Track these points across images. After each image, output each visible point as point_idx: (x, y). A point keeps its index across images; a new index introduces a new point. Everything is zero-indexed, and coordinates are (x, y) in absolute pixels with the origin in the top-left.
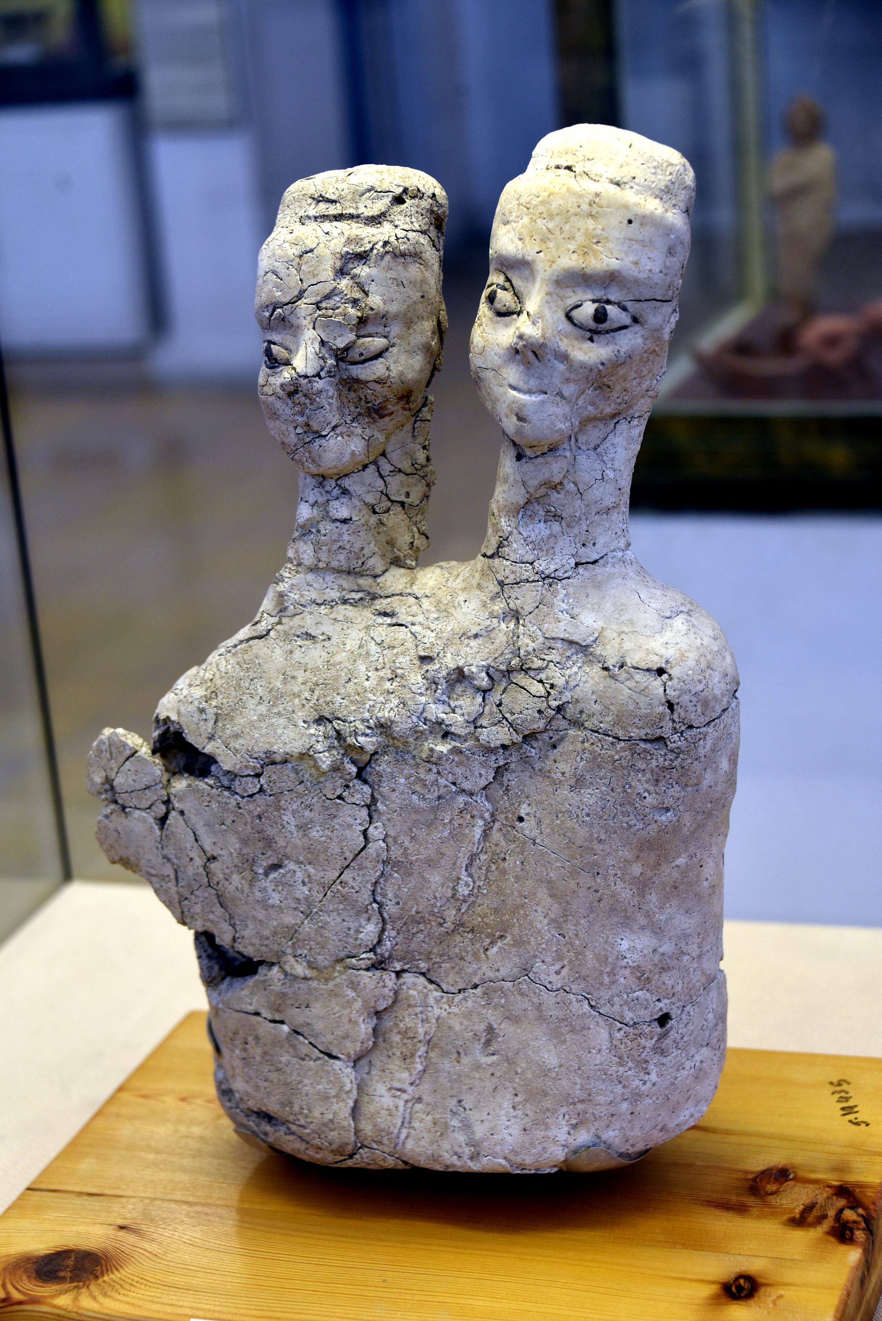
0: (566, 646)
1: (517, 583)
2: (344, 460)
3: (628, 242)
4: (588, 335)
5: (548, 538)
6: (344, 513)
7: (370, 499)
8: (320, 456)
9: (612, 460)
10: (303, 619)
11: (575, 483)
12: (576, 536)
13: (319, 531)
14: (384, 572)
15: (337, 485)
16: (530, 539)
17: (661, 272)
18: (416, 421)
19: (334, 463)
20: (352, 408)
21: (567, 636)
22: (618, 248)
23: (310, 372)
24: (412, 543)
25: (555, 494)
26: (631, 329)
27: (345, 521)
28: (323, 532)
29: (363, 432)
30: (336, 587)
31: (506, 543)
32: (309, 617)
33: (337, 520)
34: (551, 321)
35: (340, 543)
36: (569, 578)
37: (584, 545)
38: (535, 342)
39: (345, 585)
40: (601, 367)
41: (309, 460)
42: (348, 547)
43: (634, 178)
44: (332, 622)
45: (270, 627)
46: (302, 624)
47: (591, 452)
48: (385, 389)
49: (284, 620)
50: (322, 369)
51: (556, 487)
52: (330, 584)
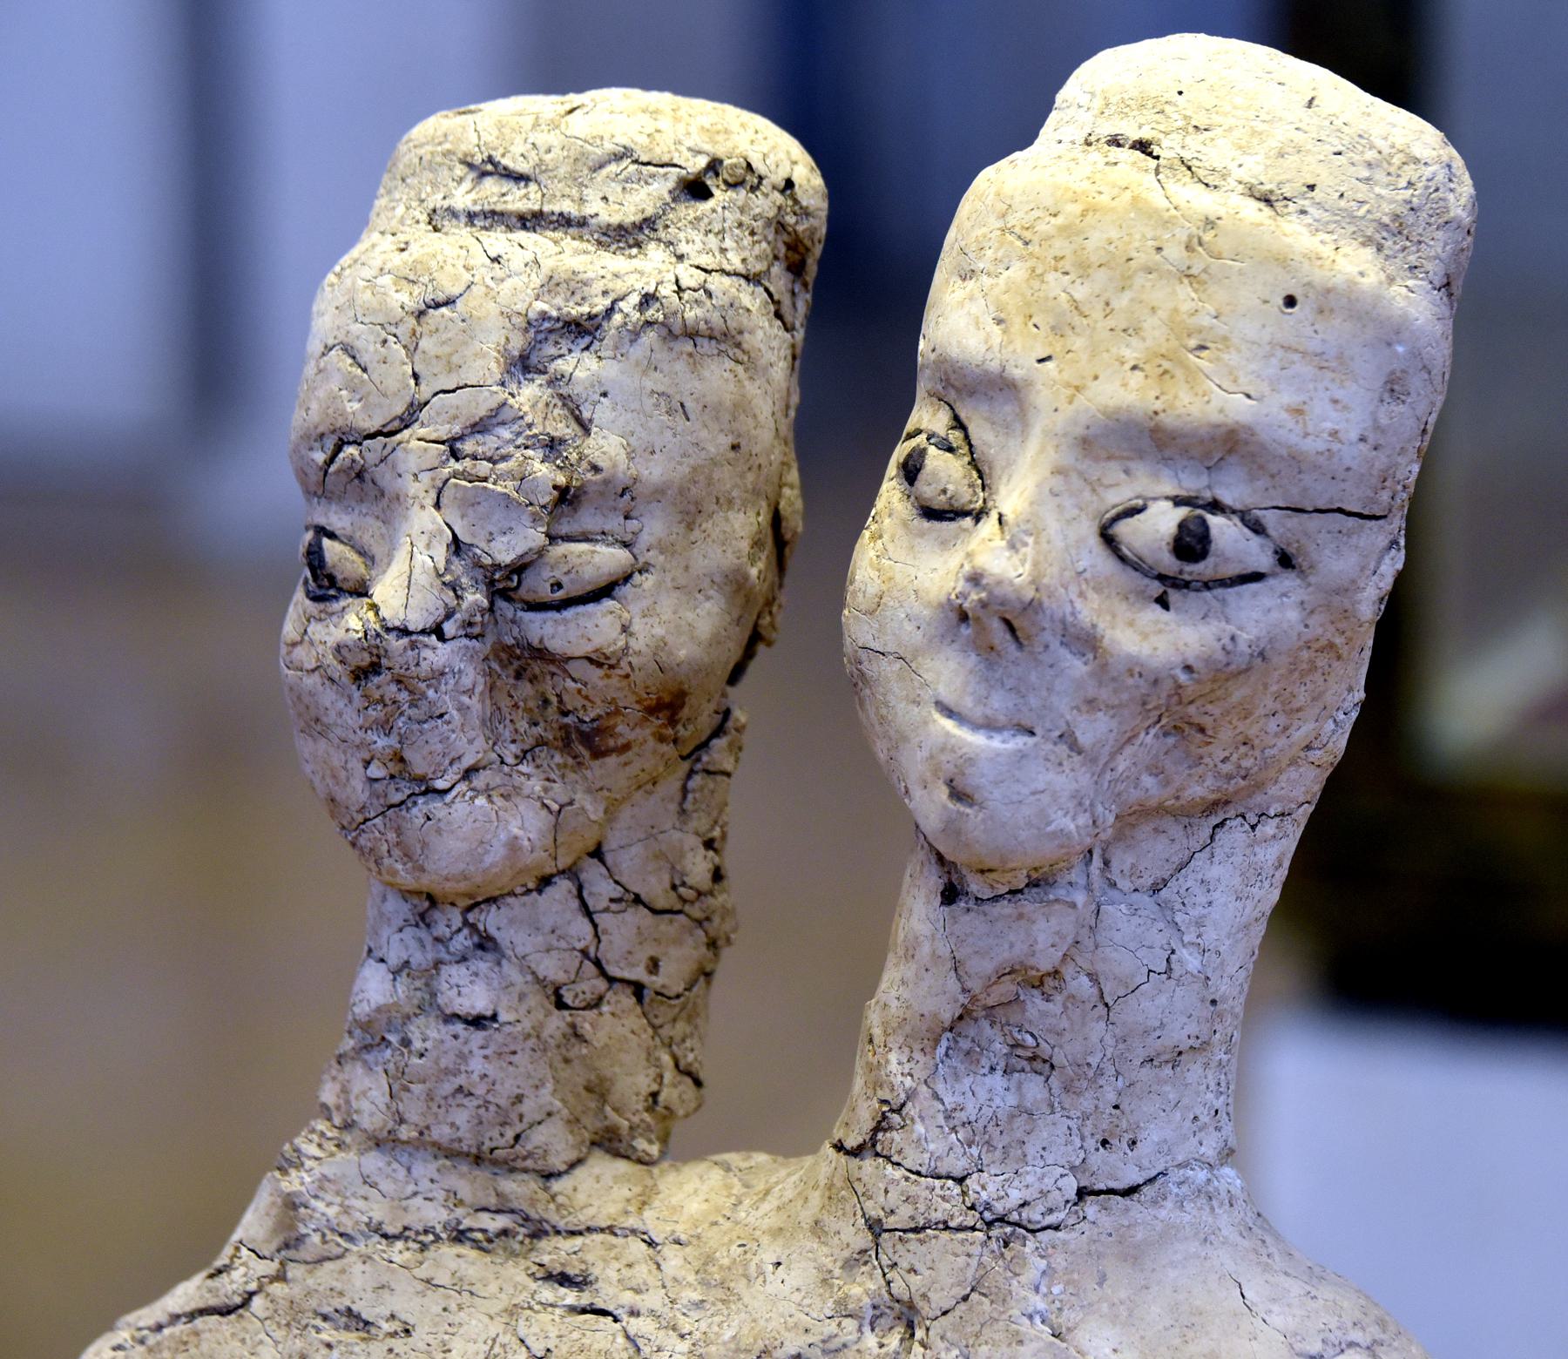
1: (916, 1230)
2: (488, 860)
3: (1280, 353)
4: (1156, 588)
5: (1012, 1117)
6: (477, 1000)
7: (551, 968)
9: (1199, 923)
10: (343, 1271)
13: (406, 1042)
14: (572, 1166)
16: (962, 1116)
17: (1362, 439)
19: (462, 866)
20: (523, 725)
22: (1253, 366)
23: (416, 621)
24: (654, 1095)
25: (1038, 1000)
26: (1271, 582)
27: (477, 1022)
28: (417, 1045)
29: (546, 790)
32: (359, 1267)
34: (1059, 544)
35: (461, 1080)
36: (1057, 1228)
37: (1105, 1143)
38: (1013, 596)
39: (465, 1191)
40: (1183, 678)
42: (480, 1090)
43: (1312, 187)
44: (420, 1286)
45: (253, 1286)
46: (338, 1286)
47: (1144, 899)
48: (615, 681)
49: (294, 1271)
51: (1044, 982)
52: (425, 1185)
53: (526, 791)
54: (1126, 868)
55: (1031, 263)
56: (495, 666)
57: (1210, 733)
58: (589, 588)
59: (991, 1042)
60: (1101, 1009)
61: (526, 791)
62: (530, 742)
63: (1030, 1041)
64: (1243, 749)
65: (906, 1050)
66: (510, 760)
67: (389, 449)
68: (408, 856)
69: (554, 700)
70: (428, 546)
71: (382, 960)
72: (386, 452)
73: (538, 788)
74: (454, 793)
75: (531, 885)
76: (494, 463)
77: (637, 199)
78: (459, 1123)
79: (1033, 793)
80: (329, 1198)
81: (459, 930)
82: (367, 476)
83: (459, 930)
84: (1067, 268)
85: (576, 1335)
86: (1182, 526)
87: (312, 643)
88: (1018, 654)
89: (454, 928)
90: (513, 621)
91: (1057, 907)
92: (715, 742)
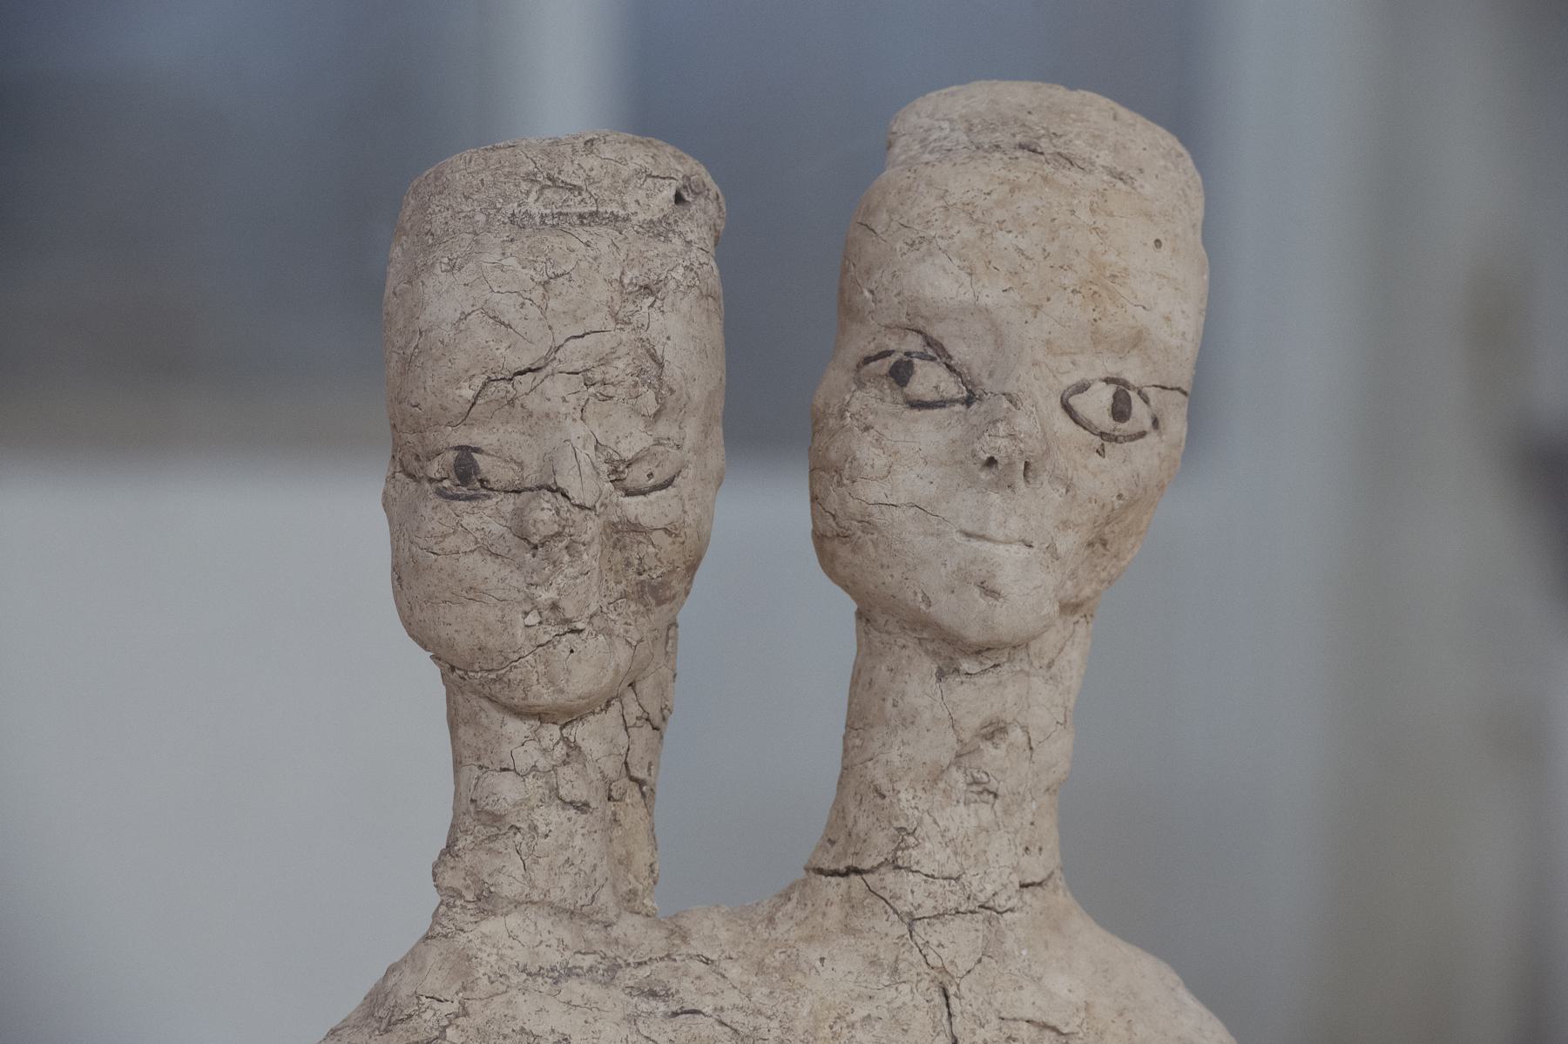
0: (1034, 1030)
2: (605, 681)
4: (1097, 441)
5: (976, 835)
8: (569, 671)
10: (509, 1002)
11: (1025, 729)
12: (1016, 832)
21: (1038, 1014)
28: (542, 829)
30: (554, 943)
31: (911, 840)
32: (521, 999)
35: (568, 854)
36: (1012, 910)
42: (577, 862)
44: (565, 1008)
45: (445, 1023)
46: (510, 1012)
49: (473, 1007)
51: (994, 731)
52: (545, 936)
55: (979, 227)
60: (1028, 752)
62: (616, 595)
63: (985, 778)
67: (538, 381)
78: (564, 889)
80: (488, 950)
85: (685, 1028)
86: (1114, 397)
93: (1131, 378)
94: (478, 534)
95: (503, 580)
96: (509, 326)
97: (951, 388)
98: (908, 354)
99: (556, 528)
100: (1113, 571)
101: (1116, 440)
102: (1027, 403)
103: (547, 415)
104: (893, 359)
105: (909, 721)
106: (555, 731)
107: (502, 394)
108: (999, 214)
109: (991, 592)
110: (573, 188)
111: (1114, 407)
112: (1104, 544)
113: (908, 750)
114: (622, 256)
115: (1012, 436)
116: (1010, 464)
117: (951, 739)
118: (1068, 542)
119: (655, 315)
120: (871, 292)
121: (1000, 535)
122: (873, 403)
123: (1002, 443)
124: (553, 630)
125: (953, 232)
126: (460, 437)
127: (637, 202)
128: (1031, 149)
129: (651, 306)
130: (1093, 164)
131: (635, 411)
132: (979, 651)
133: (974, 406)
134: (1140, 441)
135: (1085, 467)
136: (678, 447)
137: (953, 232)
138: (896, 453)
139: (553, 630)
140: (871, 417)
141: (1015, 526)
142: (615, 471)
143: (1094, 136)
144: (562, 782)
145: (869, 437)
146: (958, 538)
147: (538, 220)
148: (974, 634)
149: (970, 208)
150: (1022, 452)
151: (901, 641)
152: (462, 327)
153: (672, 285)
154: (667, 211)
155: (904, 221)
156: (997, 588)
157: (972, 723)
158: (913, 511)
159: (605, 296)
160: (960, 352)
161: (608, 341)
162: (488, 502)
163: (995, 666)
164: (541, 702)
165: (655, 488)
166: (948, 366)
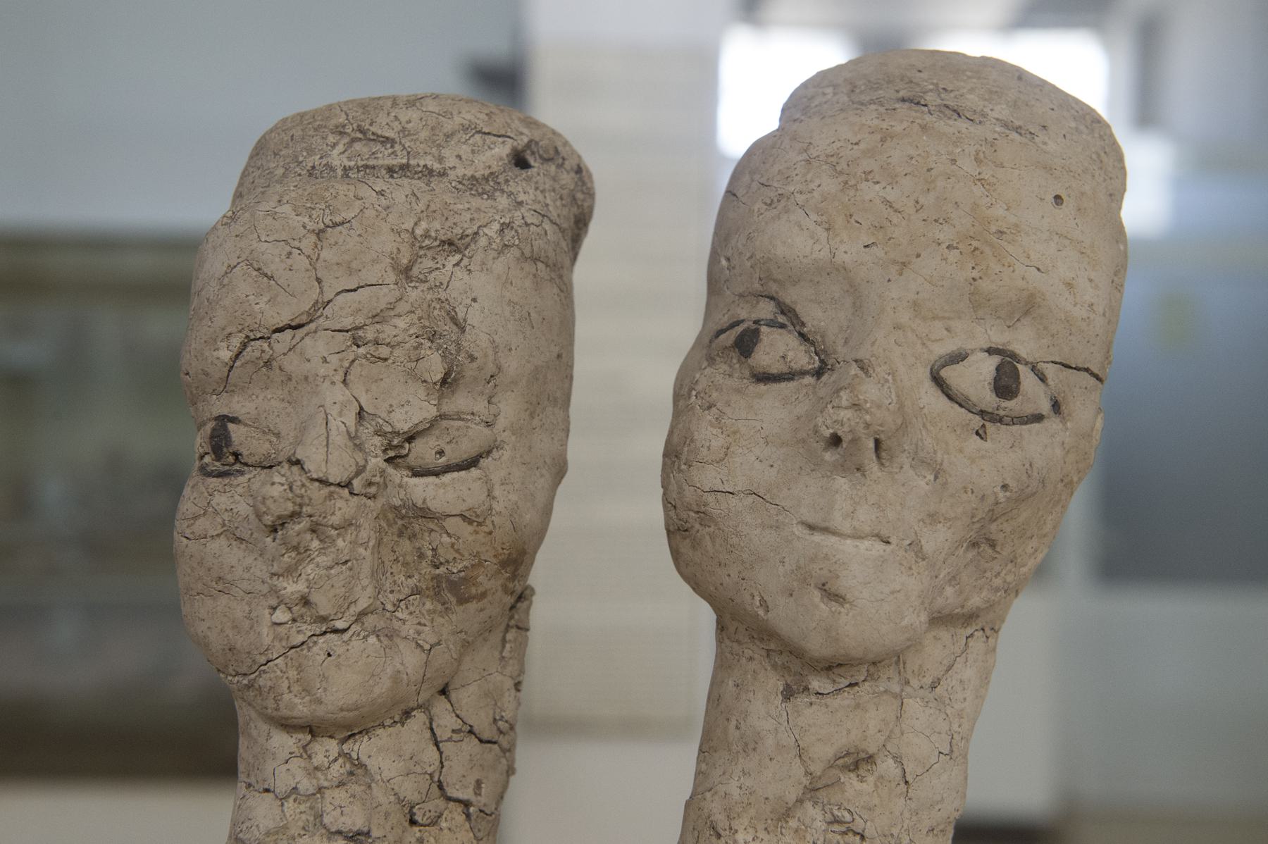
2: (377, 690)
3: (1056, 238)
4: (977, 421)
7: (410, 790)
8: (324, 678)
11: (898, 759)
15: (341, 754)
18: (508, 627)
19: (355, 697)
33: (339, 832)
40: (1002, 495)
41: (296, 688)
48: (481, 537)
50: (358, 474)
51: (857, 761)
53: (403, 634)
54: (916, 668)
55: (841, 179)
56: (384, 524)
57: (998, 549)
58: (465, 456)
59: (813, 820)
61: (403, 634)
62: (407, 591)
63: (848, 817)
64: (1010, 566)
65: (751, 830)
66: (389, 607)
67: (298, 338)
68: (307, 691)
69: (430, 553)
70: (340, 414)
71: (267, 791)
72: (294, 342)
73: (411, 632)
74: (350, 632)
75: (397, 718)
76: (393, 347)
77: (484, 159)
79: (892, 593)
81: (336, 760)
82: (274, 363)
83: (336, 760)
84: (877, 178)
87: (216, 512)
88: (879, 474)
89: (331, 758)
90: (400, 486)
91: (885, 697)
92: (519, 605)
93: (1022, 351)
94: (226, 516)
95: (248, 569)
96: (271, 278)
97: (801, 358)
98: (756, 322)
99: (290, 507)
100: (1010, 578)
101: (1001, 421)
102: (881, 371)
103: (306, 378)
104: (739, 329)
105: (750, 746)
106: (332, 746)
107: (257, 354)
108: (867, 164)
109: (833, 596)
110: (387, 140)
111: (996, 380)
112: (993, 544)
113: (748, 782)
114: (422, 206)
115: (856, 406)
116: (855, 441)
117: (798, 770)
118: (936, 540)
119: (460, 273)
120: (728, 259)
121: (846, 527)
122: (719, 379)
123: (846, 414)
124: (308, 629)
125: (812, 186)
126: (219, 406)
127: (459, 157)
128: (915, 102)
129: (457, 264)
130: (984, 115)
131: (412, 375)
132: (830, 667)
133: (825, 378)
134: (1036, 426)
135: (961, 451)
136: (488, 424)
137: (812, 186)
138: (735, 433)
139: (308, 629)
140: (715, 395)
141: (866, 517)
142: (391, 446)
143: (991, 92)
144: (329, 808)
145: (709, 416)
146: (799, 530)
147: (340, 172)
148: (816, 646)
149: (834, 160)
150: (868, 426)
151: (748, 653)
152: (226, 281)
153: (483, 241)
154: (495, 169)
155: (763, 180)
156: (842, 591)
157: (823, 752)
158: (751, 498)
159: (390, 247)
160: (814, 317)
161: (385, 296)
162: (241, 479)
163: (851, 685)
164: (295, 713)
165: (448, 469)
166: (802, 335)
